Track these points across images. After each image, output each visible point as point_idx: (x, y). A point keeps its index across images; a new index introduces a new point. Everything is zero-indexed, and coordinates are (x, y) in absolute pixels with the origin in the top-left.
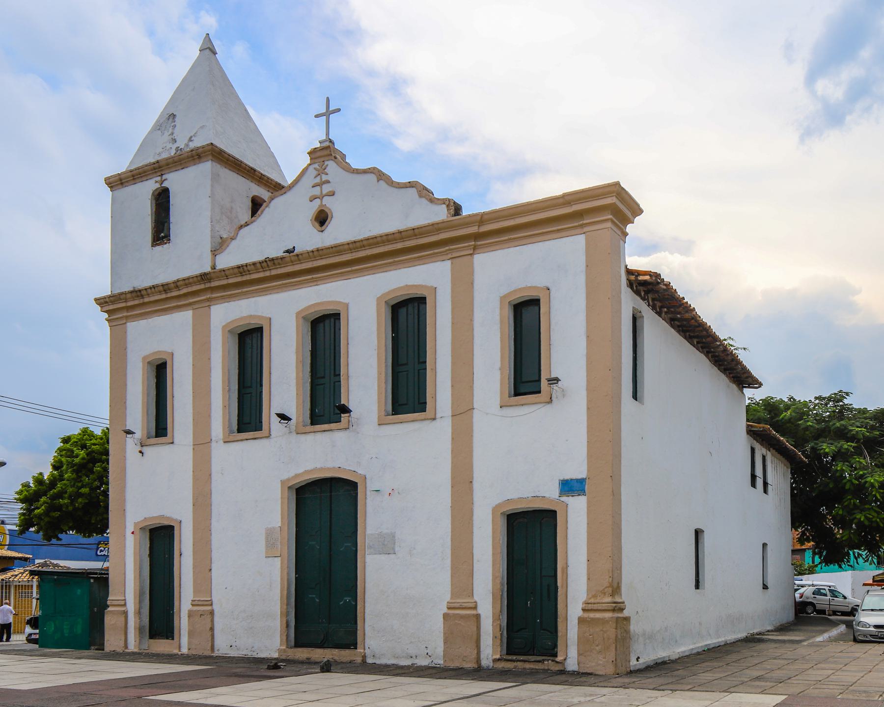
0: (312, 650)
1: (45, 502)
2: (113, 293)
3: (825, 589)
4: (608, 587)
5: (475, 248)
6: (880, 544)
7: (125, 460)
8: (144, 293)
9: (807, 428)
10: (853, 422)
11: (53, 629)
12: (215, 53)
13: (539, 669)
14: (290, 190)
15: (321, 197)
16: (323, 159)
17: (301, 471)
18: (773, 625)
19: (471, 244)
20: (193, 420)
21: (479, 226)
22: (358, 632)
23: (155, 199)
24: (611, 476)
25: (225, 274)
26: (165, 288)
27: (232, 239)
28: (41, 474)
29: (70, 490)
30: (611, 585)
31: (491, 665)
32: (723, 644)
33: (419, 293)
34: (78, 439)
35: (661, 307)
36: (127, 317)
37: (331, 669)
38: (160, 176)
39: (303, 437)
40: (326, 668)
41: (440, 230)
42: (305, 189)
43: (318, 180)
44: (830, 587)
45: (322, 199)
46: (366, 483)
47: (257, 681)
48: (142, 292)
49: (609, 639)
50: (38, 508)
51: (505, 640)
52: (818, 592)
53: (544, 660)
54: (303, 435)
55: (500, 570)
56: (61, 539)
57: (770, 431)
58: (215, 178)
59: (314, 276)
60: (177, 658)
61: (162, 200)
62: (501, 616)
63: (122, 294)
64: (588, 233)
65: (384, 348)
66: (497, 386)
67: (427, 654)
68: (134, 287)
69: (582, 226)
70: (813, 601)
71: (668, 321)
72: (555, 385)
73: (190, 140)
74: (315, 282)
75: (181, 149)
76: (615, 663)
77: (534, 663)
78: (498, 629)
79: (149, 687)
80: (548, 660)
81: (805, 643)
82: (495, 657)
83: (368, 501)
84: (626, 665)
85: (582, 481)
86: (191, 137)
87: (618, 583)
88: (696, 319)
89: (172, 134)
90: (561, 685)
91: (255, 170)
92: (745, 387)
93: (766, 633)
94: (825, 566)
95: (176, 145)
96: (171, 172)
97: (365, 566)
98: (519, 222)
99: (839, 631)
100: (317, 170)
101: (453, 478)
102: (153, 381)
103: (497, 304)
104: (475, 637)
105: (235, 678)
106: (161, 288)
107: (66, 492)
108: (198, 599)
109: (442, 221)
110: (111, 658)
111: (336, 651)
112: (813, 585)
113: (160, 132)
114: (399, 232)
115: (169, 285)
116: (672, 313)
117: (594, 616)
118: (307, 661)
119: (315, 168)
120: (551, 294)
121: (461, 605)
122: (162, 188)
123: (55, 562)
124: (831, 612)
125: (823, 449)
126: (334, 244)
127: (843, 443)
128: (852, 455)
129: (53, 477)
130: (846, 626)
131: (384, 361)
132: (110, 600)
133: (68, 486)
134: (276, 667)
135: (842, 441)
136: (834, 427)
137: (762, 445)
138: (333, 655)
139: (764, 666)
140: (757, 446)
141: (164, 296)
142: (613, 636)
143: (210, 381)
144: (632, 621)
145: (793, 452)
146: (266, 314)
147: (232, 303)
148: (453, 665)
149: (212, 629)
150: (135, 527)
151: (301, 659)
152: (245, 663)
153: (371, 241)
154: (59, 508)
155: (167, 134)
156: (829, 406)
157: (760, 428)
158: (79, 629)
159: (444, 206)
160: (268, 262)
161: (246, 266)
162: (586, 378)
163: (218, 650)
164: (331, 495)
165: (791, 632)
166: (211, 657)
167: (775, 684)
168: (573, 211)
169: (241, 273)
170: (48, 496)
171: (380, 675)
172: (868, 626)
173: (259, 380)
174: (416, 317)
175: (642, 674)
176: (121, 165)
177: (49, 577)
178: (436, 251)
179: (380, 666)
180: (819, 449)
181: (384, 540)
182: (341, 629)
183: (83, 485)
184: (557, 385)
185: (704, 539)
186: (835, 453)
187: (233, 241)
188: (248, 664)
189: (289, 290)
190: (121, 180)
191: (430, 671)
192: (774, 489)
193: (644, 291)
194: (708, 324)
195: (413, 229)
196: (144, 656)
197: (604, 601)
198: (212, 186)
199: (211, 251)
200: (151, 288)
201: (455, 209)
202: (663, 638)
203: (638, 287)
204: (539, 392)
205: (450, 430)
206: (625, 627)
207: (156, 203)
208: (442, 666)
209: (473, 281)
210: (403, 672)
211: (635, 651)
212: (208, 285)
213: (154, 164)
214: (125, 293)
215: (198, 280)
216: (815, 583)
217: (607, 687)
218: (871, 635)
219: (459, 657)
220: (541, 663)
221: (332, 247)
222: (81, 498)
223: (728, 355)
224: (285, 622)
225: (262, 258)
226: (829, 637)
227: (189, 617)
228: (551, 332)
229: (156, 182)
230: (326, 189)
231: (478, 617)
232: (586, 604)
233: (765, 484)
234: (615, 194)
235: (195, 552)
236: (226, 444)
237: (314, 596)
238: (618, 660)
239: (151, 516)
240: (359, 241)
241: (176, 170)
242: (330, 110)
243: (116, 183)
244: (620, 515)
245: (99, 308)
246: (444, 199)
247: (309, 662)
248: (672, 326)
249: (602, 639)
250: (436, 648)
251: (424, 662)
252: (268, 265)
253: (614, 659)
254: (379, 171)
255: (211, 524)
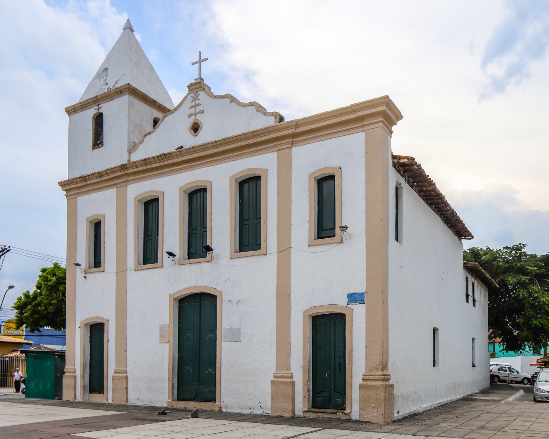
0: (188, 403)
1: (30, 309)
2: (69, 178)
3: (505, 367)
4: (380, 365)
5: (292, 143)
6: (542, 340)
7: (76, 282)
8: (87, 178)
9: (499, 267)
10: (529, 263)
11: (33, 386)
12: (133, 31)
13: (333, 418)
14: (176, 110)
15: (195, 114)
16: (196, 90)
17: (182, 288)
18: (478, 389)
19: (290, 140)
20: (116, 257)
21: (295, 129)
22: (217, 391)
23: (95, 120)
24: (382, 291)
25: (136, 165)
26: (100, 174)
27: (140, 143)
28: (28, 292)
29: (45, 301)
30: (382, 364)
31: (302, 414)
32: (450, 402)
33: (257, 173)
34: (51, 270)
35: (413, 182)
36: (77, 194)
37: (198, 416)
38: (97, 105)
39: (183, 267)
40: (195, 415)
41: (270, 132)
42: (186, 110)
43: (193, 104)
44: (507, 366)
45: (196, 116)
46: (222, 296)
47: (149, 423)
48: (86, 178)
49: (380, 399)
50: (26, 313)
51: (311, 402)
52: (501, 369)
53: (336, 412)
54: (183, 266)
55: (308, 352)
56: (41, 332)
57: (478, 266)
58: (131, 105)
59: (190, 164)
60: (104, 406)
61: (99, 120)
62: (308, 383)
63: (74, 179)
64: (366, 131)
65: (234, 209)
66: (307, 233)
67: (260, 407)
68: (81, 175)
69: (363, 126)
70: (498, 375)
71: (418, 192)
72: (345, 231)
73: (116, 83)
74: (191, 168)
75: (111, 88)
76: (384, 415)
77: (330, 414)
78: (307, 391)
79: (78, 427)
80: (339, 412)
81: (503, 402)
82: (304, 409)
83: (224, 308)
84: (391, 416)
85: (362, 294)
86: (117, 81)
87: (386, 362)
88: (436, 191)
89: (106, 80)
90: (349, 430)
91: (156, 102)
92: (463, 239)
93: (475, 395)
94: (506, 352)
95: (108, 86)
96: (105, 102)
97: (221, 349)
98: (322, 125)
99: (520, 394)
100: (192, 97)
101: (278, 292)
102: (93, 233)
103: (307, 179)
104: (291, 396)
105: (136, 421)
106: (98, 175)
107: (43, 303)
108: (118, 369)
109: (271, 126)
110: (64, 405)
111: (203, 404)
112: (497, 365)
113: (98, 79)
114: (244, 134)
115: (102, 173)
116: (420, 186)
117: (370, 383)
118: (185, 410)
119: (191, 96)
120: (342, 172)
121: (282, 375)
122: (99, 113)
123: (45, 346)
124: (510, 382)
125: (508, 280)
126: (203, 144)
127: (522, 276)
128: (528, 284)
129: (35, 293)
130: (524, 390)
131: (234, 218)
132: (66, 369)
133: (44, 299)
134: (164, 413)
135: (521, 275)
136: (516, 266)
137: (472, 276)
138: (200, 406)
139: (482, 418)
140: (470, 277)
141: (99, 180)
142: (383, 398)
143: (127, 232)
144: (395, 387)
145: (491, 281)
146: (161, 190)
147: (140, 183)
148: (277, 414)
149: (127, 388)
150: (81, 324)
151: (181, 408)
152: (146, 410)
153: (226, 141)
154: (39, 312)
155: (102, 80)
156: (512, 253)
157: (472, 264)
158: (48, 387)
159: (273, 117)
160: (162, 157)
161: (149, 159)
162: (365, 227)
163: (130, 401)
164: (200, 304)
165: (490, 394)
166: (126, 406)
167: (495, 432)
168: (357, 117)
169: (145, 164)
170: (32, 305)
171: (229, 420)
172: (544, 392)
173: (156, 231)
174: (255, 189)
175: (402, 423)
176: (76, 100)
177: (32, 354)
178: (267, 146)
179: (230, 413)
180: (506, 280)
181: (234, 332)
182: (206, 390)
183: (54, 298)
184: (346, 231)
185: (438, 334)
186: (517, 283)
187: (141, 144)
188: (147, 411)
189: (175, 174)
190: (74, 109)
191: (262, 418)
192: (479, 304)
193: (403, 171)
194: (443, 195)
195: (253, 132)
196: (86, 404)
197: (376, 374)
198: (129, 110)
199: (128, 151)
200: (91, 175)
201: (280, 119)
202: (414, 399)
203: (399, 168)
204: (334, 236)
205: (276, 261)
206: (391, 391)
207: (95, 122)
208: (270, 415)
209: (291, 165)
210: (244, 418)
211: (397, 407)
212: (125, 172)
213: (94, 98)
214: (76, 179)
215: (119, 169)
216: (498, 363)
217: (380, 432)
218: (546, 398)
219: (281, 409)
220: (334, 414)
221: (202, 146)
222: (52, 306)
223: (454, 216)
224: (171, 384)
225: (158, 154)
226: (516, 398)
227: (113, 380)
228: (342, 197)
229: (95, 109)
230: (199, 109)
231: (293, 383)
232: (365, 375)
233: (474, 300)
234: (385, 104)
235: (117, 339)
236: (136, 271)
237: (190, 368)
238: (386, 414)
239: (91, 317)
240: (219, 141)
241: (107, 102)
242: (201, 59)
243: (71, 111)
244: (388, 317)
245: (60, 188)
246: (272, 112)
247: (185, 410)
248: (420, 195)
249: (376, 399)
250: (266, 403)
251: (258, 412)
252: (162, 158)
253: (384, 412)
254: (232, 96)
255: (126, 322)
